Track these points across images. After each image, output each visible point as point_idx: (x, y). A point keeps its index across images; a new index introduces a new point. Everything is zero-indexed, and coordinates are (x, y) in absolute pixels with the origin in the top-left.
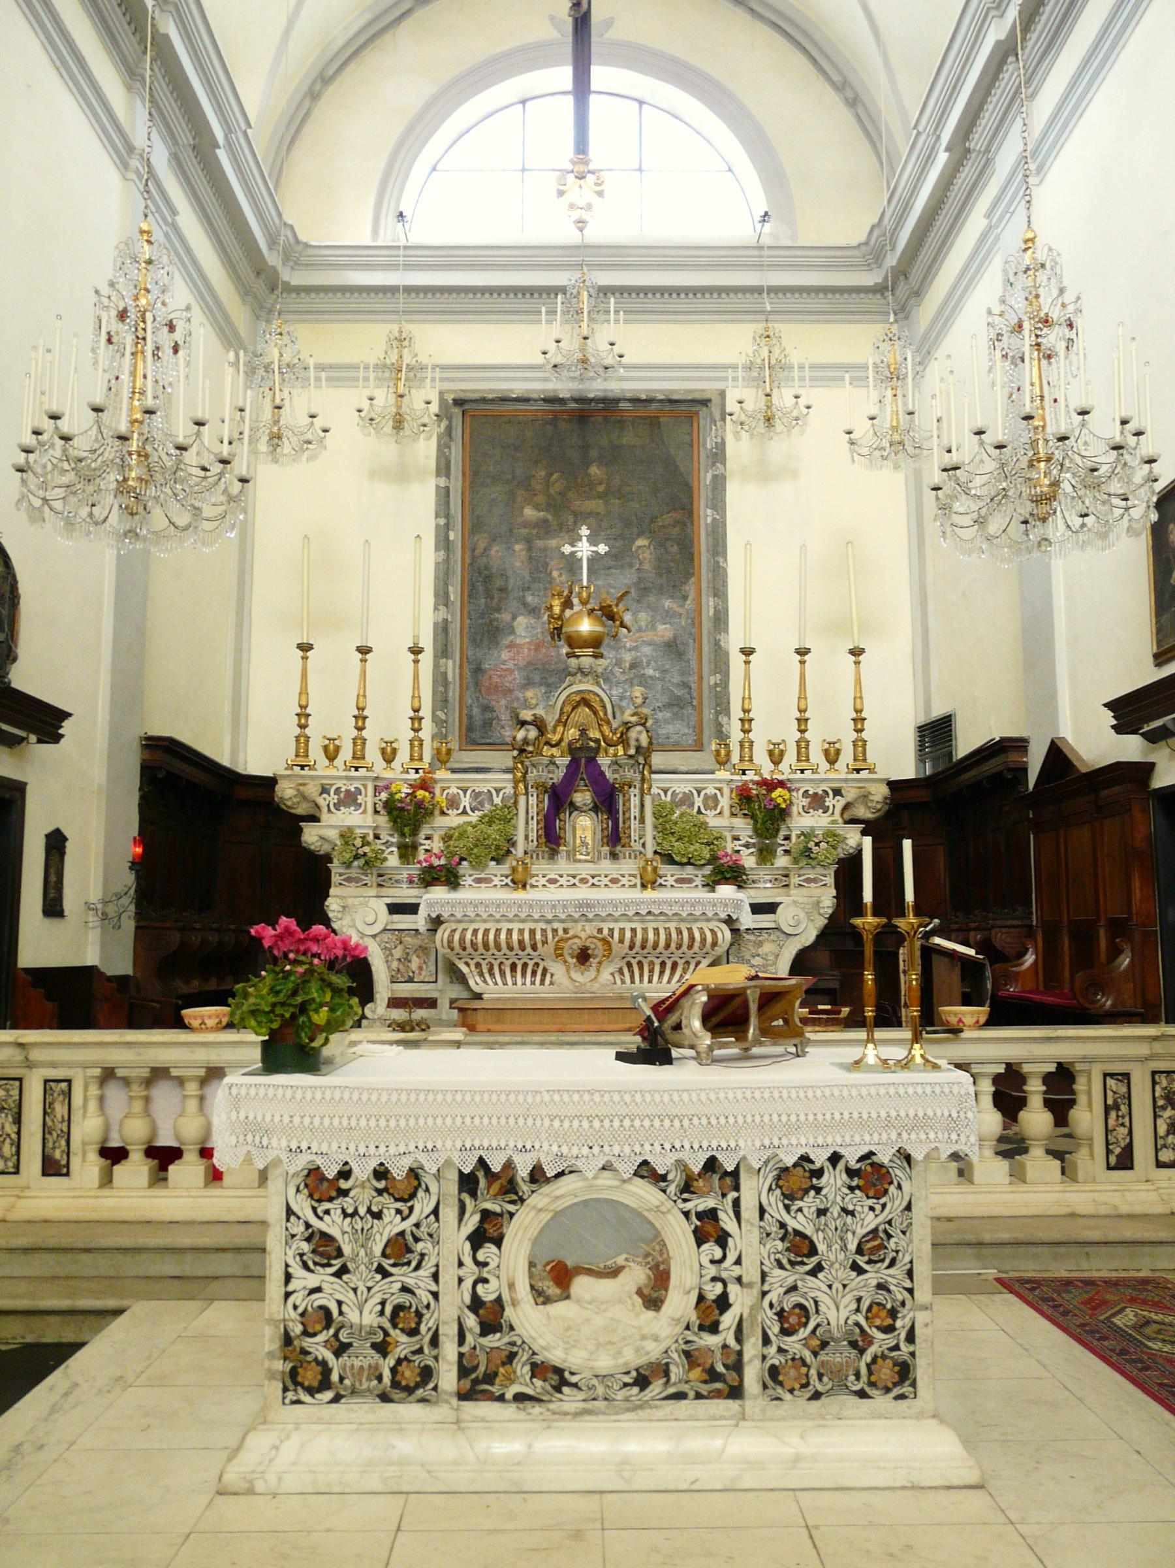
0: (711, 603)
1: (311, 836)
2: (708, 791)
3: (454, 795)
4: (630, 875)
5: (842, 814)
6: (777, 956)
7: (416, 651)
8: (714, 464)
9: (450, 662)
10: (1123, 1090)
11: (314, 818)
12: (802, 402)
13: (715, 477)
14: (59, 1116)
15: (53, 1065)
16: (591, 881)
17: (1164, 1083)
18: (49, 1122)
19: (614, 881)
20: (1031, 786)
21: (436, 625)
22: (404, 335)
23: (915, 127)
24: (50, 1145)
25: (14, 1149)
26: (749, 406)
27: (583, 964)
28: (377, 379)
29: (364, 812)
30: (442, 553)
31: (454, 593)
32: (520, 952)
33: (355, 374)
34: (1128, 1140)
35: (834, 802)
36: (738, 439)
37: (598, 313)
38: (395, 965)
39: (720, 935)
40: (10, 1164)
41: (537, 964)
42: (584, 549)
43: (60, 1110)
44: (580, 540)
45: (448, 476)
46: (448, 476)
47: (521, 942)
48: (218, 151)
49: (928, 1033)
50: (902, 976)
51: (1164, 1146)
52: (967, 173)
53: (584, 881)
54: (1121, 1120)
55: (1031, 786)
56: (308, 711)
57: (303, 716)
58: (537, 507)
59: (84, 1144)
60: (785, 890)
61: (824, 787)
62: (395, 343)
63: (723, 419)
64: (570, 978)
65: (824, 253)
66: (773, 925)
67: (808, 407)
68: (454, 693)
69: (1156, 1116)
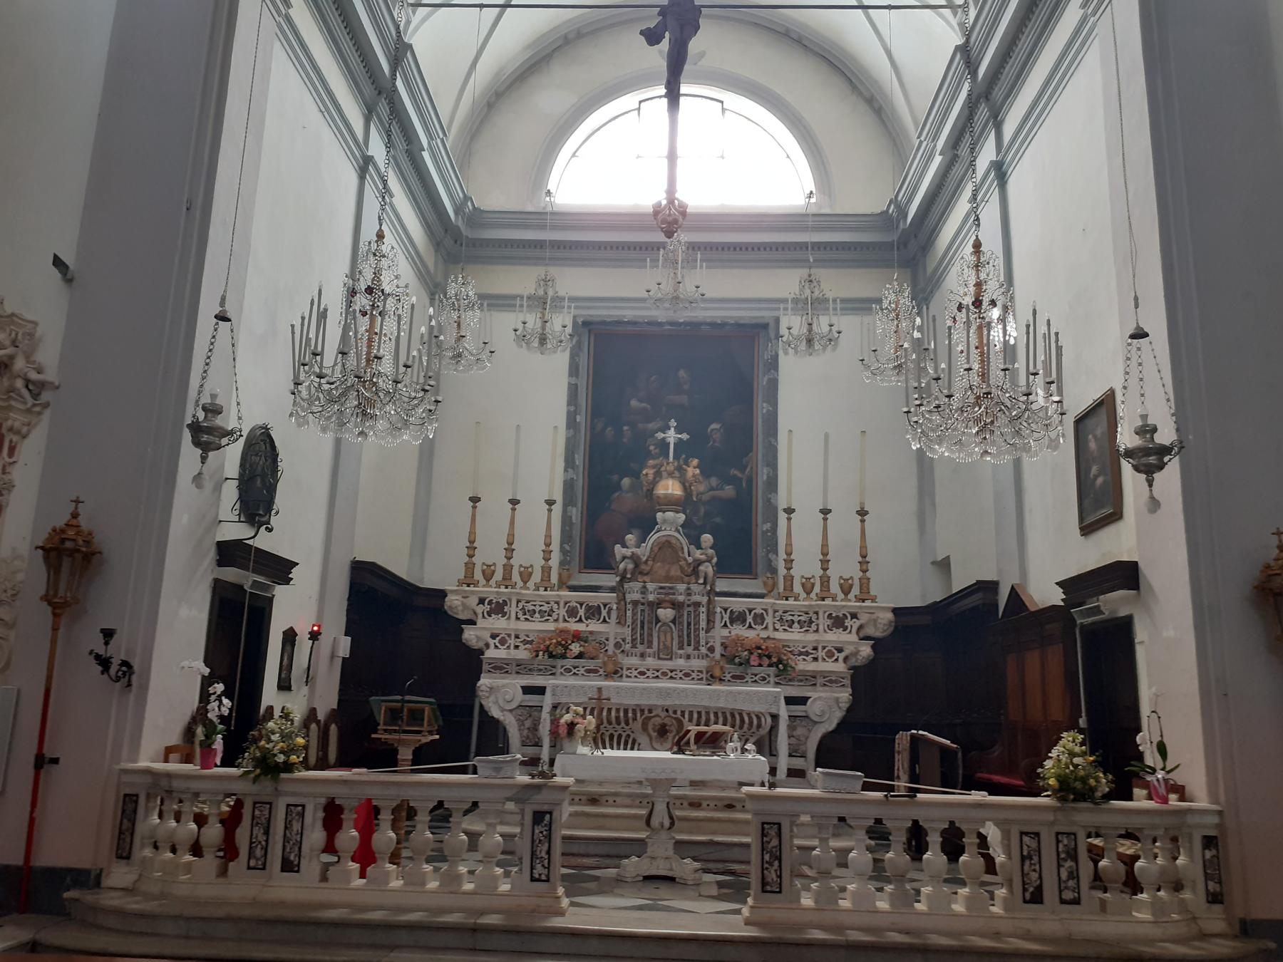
0: (765, 471)
4: (699, 671)
6: (807, 738)
7: (550, 503)
8: (769, 370)
9: (574, 510)
10: (1034, 845)
11: (472, 622)
13: (769, 380)
14: (295, 830)
15: (294, 794)
16: (670, 674)
17: (1065, 842)
18: (288, 835)
19: (687, 675)
21: (565, 482)
24: (288, 850)
25: (263, 852)
26: (795, 331)
27: (662, 737)
28: (528, 306)
29: (509, 618)
30: (571, 430)
31: (579, 460)
33: (513, 302)
34: (1038, 882)
35: (851, 623)
36: (786, 353)
37: (690, 263)
38: (525, 732)
39: (763, 720)
40: (260, 863)
41: (628, 736)
42: (672, 436)
43: (296, 826)
45: (577, 377)
46: (577, 377)
47: (617, 718)
48: (423, 153)
49: (892, 796)
50: (896, 755)
51: (1066, 888)
52: (957, 171)
53: (664, 674)
54: (1033, 867)
56: (475, 545)
57: (471, 550)
58: (641, 401)
59: (312, 850)
60: (813, 687)
62: (542, 283)
66: (804, 714)
67: (839, 333)
68: (576, 532)
69: (1059, 866)
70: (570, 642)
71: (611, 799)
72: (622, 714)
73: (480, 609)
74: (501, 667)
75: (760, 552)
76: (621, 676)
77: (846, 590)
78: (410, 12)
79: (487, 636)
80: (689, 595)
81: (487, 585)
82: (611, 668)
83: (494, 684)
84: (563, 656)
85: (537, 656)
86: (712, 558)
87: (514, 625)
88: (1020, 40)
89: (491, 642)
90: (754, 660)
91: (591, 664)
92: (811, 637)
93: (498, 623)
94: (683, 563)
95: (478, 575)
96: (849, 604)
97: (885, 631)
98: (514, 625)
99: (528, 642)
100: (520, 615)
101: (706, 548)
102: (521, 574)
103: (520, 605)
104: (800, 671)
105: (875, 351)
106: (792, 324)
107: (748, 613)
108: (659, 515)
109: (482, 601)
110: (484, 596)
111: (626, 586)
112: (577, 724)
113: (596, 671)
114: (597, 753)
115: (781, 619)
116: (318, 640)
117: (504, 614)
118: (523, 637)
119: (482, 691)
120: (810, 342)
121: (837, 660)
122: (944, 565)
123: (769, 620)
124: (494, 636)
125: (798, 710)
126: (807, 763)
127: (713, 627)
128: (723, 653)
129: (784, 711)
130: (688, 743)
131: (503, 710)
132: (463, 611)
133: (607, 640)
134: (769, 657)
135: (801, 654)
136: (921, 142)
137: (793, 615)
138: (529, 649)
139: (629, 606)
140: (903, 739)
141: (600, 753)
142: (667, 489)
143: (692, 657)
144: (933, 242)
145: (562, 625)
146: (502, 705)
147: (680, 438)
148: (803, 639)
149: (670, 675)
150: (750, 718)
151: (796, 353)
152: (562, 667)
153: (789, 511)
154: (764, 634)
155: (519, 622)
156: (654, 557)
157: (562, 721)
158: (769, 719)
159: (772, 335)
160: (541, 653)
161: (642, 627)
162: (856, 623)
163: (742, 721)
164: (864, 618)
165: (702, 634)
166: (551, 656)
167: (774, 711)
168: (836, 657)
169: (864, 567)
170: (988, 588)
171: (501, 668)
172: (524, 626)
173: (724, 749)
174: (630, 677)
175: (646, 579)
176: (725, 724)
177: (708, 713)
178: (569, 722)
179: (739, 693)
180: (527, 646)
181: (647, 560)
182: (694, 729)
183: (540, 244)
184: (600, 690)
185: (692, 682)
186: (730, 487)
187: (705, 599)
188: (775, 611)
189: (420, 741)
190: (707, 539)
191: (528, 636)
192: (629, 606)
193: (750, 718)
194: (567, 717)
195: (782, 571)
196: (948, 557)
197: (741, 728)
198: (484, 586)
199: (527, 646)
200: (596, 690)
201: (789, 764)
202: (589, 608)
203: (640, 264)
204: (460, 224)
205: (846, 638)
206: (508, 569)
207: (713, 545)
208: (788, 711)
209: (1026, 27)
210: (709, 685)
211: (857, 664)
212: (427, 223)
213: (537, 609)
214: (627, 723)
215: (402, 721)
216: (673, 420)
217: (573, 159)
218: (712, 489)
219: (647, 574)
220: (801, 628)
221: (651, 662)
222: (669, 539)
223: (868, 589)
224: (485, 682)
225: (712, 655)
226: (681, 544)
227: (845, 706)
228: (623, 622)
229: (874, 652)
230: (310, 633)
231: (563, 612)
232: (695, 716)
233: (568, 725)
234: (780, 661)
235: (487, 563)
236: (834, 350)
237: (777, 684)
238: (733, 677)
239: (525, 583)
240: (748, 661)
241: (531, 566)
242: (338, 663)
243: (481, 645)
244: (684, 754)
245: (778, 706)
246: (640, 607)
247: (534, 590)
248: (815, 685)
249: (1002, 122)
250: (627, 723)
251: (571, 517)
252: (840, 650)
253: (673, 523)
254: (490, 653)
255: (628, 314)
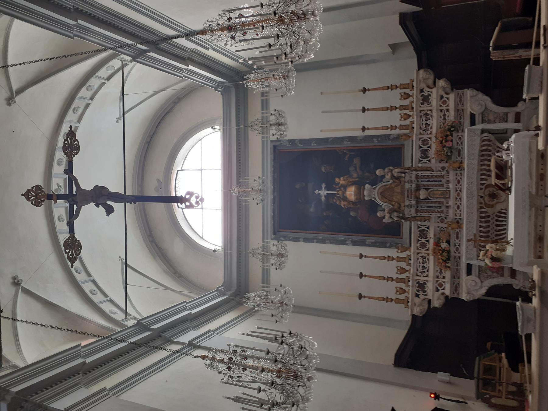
1: (437, 303)
2: (420, 144)
3: (421, 245)
5: (431, 88)
6: (495, 113)
7: (361, 256)
8: (295, 144)
9: (368, 240)
11: (429, 301)
12: (273, 112)
13: (300, 143)
19: (459, 182)
20: (421, 9)
21: (353, 245)
22: (252, 252)
23: (182, 77)
29: (427, 281)
31: (341, 238)
32: (491, 223)
36: (286, 136)
37: (246, 184)
41: (497, 216)
44: (320, 193)
45: (300, 238)
46: (300, 238)
47: (486, 222)
50: (506, 59)
52: (196, 58)
53: (458, 195)
55: (421, 9)
57: (387, 300)
61: (419, 97)
63: (280, 141)
64: (503, 202)
65: (225, 107)
66: (481, 116)
68: (380, 239)
70: (440, 248)
71: (539, 228)
72: (483, 220)
73: (422, 297)
74: (456, 287)
75: (389, 143)
76: (460, 219)
77: (407, 96)
78: (130, 317)
79: (437, 294)
80: (411, 181)
81: (408, 292)
82: (455, 225)
83: (466, 291)
84: (449, 252)
85: (449, 267)
86: (390, 169)
87: (431, 279)
88: (125, 29)
89: (441, 291)
90: (449, 144)
91: (453, 236)
92: (435, 114)
93: (430, 287)
94: (393, 185)
95: (402, 297)
96: (415, 94)
97: (430, 73)
98: (431, 279)
99: (441, 270)
100: (425, 275)
101: (385, 173)
102: (401, 273)
103: (420, 274)
104: (455, 118)
105: (276, 90)
106: (273, 134)
107: (422, 149)
108: (366, 198)
109: (417, 296)
110: (414, 295)
111: (407, 216)
112: (491, 255)
113: (457, 234)
114: (512, 242)
115: (425, 130)
116: (439, 395)
117: (425, 284)
118: (438, 274)
119: (470, 298)
120: (280, 125)
121: (448, 98)
122: (394, 47)
123: (425, 137)
124: (438, 290)
125: (478, 118)
126: (512, 111)
127: (430, 167)
128: (445, 162)
129: (479, 126)
130: (503, 184)
131: (481, 287)
132: (423, 306)
133: (439, 227)
134: (447, 136)
135: (445, 119)
136: (184, 76)
137: (423, 124)
138: (445, 271)
139: (419, 214)
140: (496, 56)
141: (511, 241)
142: (352, 194)
143: (448, 179)
144: (233, 68)
145: (430, 252)
146: (478, 288)
147: (325, 188)
148: (436, 118)
149: (459, 192)
150: (484, 145)
151: (285, 131)
152: (455, 253)
153: (364, 129)
154: (434, 139)
155: (429, 276)
156: (390, 201)
157: (490, 265)
158: (485, 135)
159: (279, 143)
160: (447, 265)
161: (431, 207)
162: (427, 90)
163: (486, 150)
164: (423, 85)
165: (434, 173)
166: (448, 259)
167: (479, 132)
168: (446, 99)
169: (394, 87)
170: (404, 19)
171: (456, 287)
172: (431, 273)
173: (507, 162)
174: (461, 214)
175: (402, 205)
176: (490, 160)
177: (482, 170)
178: (490, 260)
179: (469, 152)
180: (443, 272)
181: (392, 205)
182: (493, 180)
183: (239, 256)
184: (469, 240)
185: (463, 178)
186: (354, 160)
187: (414, 173)
188: (421, 134)
189: (507, 369)
190: (378, 172)
191: (437, 271)
192: (419, 214)
193: (484, 145)
194: (487, 261)
195: (397, 131)
196: (389, 45)
197: (490, 151)
198: (409, 294)
199: (443, 272)
200: (469, 243)
201: (512, 122)
202: (421, 236)
203: (247, 208)
204: (229, 293)
205: (434, 94)
206: (399, 280)
207: (383, 169)
208: (479, 124)
209: (118, 26)
210: (464, 169)
211: (450, 87)
212: (230, 309)
213: (421, 265)
214: (489, 217)
215: (493, 380)
216: (315, 192)
217: (203, 238)
218: (356, 170)
219: (400, 205)
220: (430, 119)
221: (451, 203)
222: (379, 193)
223: (406, 84)
224: (464, 296)
225: (447, 168)
226: (382, 186)
227: (475, 92)
228: (428, 218)
229: (442, 78)
230: (435, 399)
231: (423, 251)
232: (483, 177)
233: (493, 261)
234: (449, 130)
235: (396, 292)
236: (284, 112)
237: (463, 131)
238: (459, 156)
239: (406, 271)
240: (449, 148)
241: (397, 267)
242: (455, 379)
243: (442, 297)
244: (511, 187)
245: (476, 129)
246: (419, 208)
247: (411, 266)
248: (463, 110)
249: (168, 36)
250: (489, 217)
251: (372, 242)
252: (442, 97)
253: (370, 191)
254: (447, 292)
255: (270, 213)
